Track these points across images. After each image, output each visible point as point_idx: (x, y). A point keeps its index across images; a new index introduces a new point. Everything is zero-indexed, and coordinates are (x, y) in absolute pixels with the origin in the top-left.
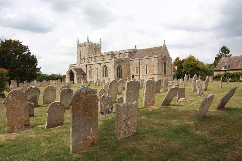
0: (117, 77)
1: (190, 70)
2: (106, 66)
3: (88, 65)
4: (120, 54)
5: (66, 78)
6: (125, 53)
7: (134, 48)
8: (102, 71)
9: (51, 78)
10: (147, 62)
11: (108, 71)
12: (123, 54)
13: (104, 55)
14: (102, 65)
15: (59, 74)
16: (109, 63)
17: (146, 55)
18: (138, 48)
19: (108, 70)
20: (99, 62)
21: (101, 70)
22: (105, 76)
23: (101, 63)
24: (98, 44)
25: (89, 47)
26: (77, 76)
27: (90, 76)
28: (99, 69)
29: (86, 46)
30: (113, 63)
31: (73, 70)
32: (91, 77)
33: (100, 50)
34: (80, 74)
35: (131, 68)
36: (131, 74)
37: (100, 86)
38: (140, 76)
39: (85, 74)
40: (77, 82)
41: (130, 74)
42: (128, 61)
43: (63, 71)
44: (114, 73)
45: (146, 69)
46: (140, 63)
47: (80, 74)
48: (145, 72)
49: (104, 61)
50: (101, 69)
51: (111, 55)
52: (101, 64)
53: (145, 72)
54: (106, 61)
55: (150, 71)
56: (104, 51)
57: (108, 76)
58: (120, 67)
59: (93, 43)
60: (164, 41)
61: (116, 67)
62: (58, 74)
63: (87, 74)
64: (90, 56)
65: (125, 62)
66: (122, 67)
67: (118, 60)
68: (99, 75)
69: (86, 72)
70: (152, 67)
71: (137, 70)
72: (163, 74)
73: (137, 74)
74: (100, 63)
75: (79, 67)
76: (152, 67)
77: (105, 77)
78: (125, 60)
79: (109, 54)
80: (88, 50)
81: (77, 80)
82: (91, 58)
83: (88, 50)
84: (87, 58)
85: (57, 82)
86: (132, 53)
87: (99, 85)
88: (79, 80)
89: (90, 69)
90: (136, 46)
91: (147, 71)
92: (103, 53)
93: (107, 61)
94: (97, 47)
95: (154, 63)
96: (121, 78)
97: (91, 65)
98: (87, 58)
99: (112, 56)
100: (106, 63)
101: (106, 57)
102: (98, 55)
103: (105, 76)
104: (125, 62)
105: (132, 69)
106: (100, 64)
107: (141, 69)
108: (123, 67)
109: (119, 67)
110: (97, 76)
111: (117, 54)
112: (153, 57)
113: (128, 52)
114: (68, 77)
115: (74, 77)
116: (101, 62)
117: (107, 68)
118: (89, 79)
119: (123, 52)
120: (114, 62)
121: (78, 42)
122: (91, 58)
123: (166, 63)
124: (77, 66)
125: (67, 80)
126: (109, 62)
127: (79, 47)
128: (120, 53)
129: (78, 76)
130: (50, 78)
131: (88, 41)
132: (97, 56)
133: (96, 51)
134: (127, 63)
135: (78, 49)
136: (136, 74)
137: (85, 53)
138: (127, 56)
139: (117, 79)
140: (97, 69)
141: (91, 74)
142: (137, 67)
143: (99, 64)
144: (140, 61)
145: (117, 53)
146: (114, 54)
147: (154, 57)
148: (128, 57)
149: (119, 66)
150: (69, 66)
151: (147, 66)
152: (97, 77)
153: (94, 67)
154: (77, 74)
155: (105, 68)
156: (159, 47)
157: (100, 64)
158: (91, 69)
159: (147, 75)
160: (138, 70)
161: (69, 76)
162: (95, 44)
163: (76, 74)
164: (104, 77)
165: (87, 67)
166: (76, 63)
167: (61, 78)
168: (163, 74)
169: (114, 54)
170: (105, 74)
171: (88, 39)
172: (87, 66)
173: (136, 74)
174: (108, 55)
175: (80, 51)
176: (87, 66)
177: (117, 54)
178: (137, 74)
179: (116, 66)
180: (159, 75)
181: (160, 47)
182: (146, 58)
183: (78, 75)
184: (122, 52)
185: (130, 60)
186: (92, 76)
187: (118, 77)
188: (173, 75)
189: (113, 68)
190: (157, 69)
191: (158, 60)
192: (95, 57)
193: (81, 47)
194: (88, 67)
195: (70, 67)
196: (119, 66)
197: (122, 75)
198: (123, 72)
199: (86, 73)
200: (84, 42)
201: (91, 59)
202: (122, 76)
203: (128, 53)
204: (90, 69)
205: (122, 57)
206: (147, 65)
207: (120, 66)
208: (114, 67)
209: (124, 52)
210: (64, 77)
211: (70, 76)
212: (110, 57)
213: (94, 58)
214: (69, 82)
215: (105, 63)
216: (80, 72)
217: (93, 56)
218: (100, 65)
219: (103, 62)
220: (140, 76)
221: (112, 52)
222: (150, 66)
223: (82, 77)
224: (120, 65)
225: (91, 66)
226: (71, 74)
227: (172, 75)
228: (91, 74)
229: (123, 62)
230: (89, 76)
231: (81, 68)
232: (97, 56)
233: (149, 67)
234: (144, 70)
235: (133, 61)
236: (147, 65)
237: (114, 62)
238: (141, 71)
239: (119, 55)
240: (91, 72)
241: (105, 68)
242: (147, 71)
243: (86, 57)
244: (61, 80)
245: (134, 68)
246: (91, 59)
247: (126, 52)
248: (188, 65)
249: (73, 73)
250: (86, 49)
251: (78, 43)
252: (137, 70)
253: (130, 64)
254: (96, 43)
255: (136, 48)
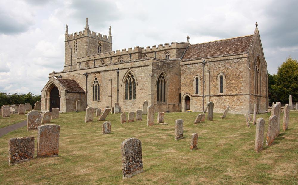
0: (157, 98)
1: (292, 88)
2: (132, 76)
3: (89, 73)
4: (156, 52)
5: (41, 100)
6: (169, 49)
7: (185, 40)
8: (122, 86)
9: (13, 99)
10: (223, 68)
11: (136, 86)
12: (163, 52)
13: (121, 54)
14: (123, 73)
15: (29, 93)
16: (140, 68)
17: (215, 54)
18: (193, 41)
19: (138, 85)
20: (116, 67)
21: (119, 85)
22: (163, 100)
23: (121, 69)
24: (105, 36)
25: (89, 41)
26: (66, 95)
27: (94, 97)
28: (115, 82)
29: (84, 39)
30: (151, 67)
31: (57, 84)
32: (96, 99)
33: (109, 48)
34: (74, 92)
35: (183, 80)
36: (183, 93)
37: (133, 121)
38: (204, 98)
39: (82, 93)
40: (66, 110)
41: (180, 94)
42: (177, 66)
43: (37, 88)
44: (152, 90)
45: (218, 83)
46: (206, 70)
47: (74, 92)
48: (217, 89)
49: (129, 64)
50: (120, 82)
51: (137, 54)
52: (120, 71)
53: (217, 89)
54: (133, 65)
55: (230, 88)
56: (117, 46)
57: (137, 97)
58: (163, 77)
59: (97, 34)
60: (257, 25)
61: (157, 76)
62: (26, 93)
63: (87, 92)
64: (92, 58)
65: (172, 67)
66: (166, 78)
67: (160, 63)
68: (115, 95)
69: (84, 89)
70: (236, 78)
71: (197, 84)
72: (255, 94)
73: (197, 92)
74: (118, 69)
75: (70, 78)
76: (234, 78)
77: (130, 98)
78: (172, 63)
79: (134, 52)
80: (87, 45)
81: (66, 104)
82: (94, 60)
83: (87, 45)
84: (84, 62)
85: (21, 109)
86: (182, 51)
87: (132, 119)
88: (71, 106)
89: (95, 82)
90: (188, 38)
91: (221, 87)
92: (114, 52)
93: (136, 63)
94: (104, 42)
95: (241, 69)
96: (164, 101)
97: (96, 73)
98: (84, 62)
99: (139, 56)
100: (133, 69)
101: (126, 58)
102: (108, 54)
103: (163, 100)
104: (172, 67)
105: (185, 82)
106: (118, 71)
107: (207, 83)
108: (168, 77)
109: (160, 76)
110: (110, 98)
111: (150, 53)
112: (237, 57)
113: (175, 48)
114: (46, 99)
115: (59, 99)
116: (121, 66)
117: (134, 80)
118: (91, 103)
119: (164, 49)
120: (152, 66)
121: (67, 31)
122: (93, 62)
123: (258, 70)
124: (65, 76)
125: (45, 106)
126: (139, 67)
127: (69, 41)
128: (157, 50)
129: (67, 97)
130: (11, 101)
131: (87, 29)
132: (107, 58)
133: (102, 50)
134: (175, 71)
135: (66, 45)
136: (195, 94)
137: (81, 52)
138: (173, 56)
139: (158, 104)
140: (111, 81)
141: (96, 92)
142: (197, 79)
143: (115, 71)
144: (206, 67)
145: (151, 51)
146: (143, 52)
147: (241, 56)
148: (174, 57)
149: (162, 76)
150: (49, 76)
151: (221, 77)
152: (111, 98)
153: (104, 79)
154: (67, 92)
155: (128, 80)
156: (244, 37)
157: (118, 71)
158: (97, 82)
159: (222, 96)
160: (200, 84)
161: (48, 97)
162: (100, 35)
163: (64, 91)
164: (126, 98)
165: (88, 78)
166: (62, 70)
167: (31, 101)
168: (257, 94)
169: (144, 52)
170: (131, 92)
171: (87, 26)
172: (86, 75)
173: (195, 94)
174: (130, 54)
175: (70, 49)
176: (86, 75)
177: (150, 53)
178: (197, 92)
179: (155, 75)
180: (251, 95)
181: (246, 37)
182: (219, 59)
183: (69, 94)
184: (161, 48)
185: (181, 63)
186: (99, 97)
187: (158, 100)
188: (268, 96)
189: (150, 79)
190: (248, 82)
191: (249, 63)
192: (102, 60)
193: (73, 41)
194: (91, 77)
195: (50, 78)
196: (162, 76)
197: (166, 95)
198: (168, 89)
199: (85, 91)
200: (80, 31)
201: (95, 63)
202: (166, 97)
203: (175, 50)
204: (95, 82)
205: (161, 56)
206: (222, 74)
207: (162, 76)
208: (153, 76)
209: (167, 48)
210: (39, 99)
211: (50, 97)
212: (135, 57)
213: (99, 61)
214: (48, 110)
215: (131, 68)
216: (73, 87)
217: (97, 57)
218: (118, 73)
219: (125, 67)
220: (204, 98)
221: (139, 48)
222: (230, 75)
223: (76, 99)
224: (162, 74)
225: (97, 75)
226: (53, 91)
227: (267, 96)
228: (96, 92)
229: (169, 68)
230: (92, 96)
231: (74, 81)
232: (107, 58)
233: (227, 79)
234: (215, 86)
235: (187, 66)
236: (222, 74)
237: (151, 65)
238: (207, 88)
239: (154, 53)
240: (96, 89)
241: (128, 80)
242: (221, 87)
243: (83, 60)
244: (31, 104)
245: (189, 81)
246: (95, 63)
247: (170, 48)
248: (289, 78)
249: (58, 90)
250: (82, 45)
251: (67, 35)
252: (197, 84)
253: (181, 72)
254: (96, 33)
255: (190, 42)
